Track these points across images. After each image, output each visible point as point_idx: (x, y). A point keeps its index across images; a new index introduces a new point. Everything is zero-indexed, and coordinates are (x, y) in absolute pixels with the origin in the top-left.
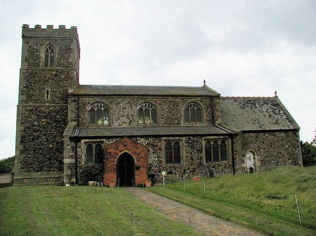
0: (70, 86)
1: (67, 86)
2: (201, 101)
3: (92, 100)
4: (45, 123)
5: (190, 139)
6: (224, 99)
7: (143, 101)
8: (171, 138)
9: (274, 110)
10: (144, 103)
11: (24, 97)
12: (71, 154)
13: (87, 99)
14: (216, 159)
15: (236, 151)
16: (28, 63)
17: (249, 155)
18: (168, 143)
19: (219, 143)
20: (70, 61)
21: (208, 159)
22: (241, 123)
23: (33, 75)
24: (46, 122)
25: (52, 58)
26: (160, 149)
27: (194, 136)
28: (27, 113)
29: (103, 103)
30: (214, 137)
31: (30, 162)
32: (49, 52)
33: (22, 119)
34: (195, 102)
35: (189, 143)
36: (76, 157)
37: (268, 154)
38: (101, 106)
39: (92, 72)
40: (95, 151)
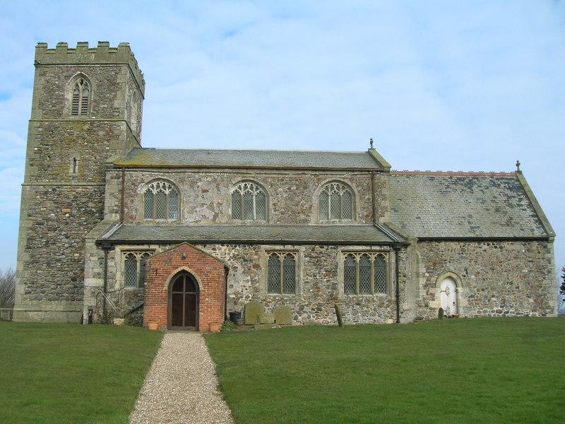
0: (115, 151)
1: (108, 151)
2: (351, 180)
3: (147, 175)
5: (313, 250)
6: (397, 174)
7: (240, 179)
8: (278, 247)
9: (509, 198)
10: (243, 181)
11: (35, 170)
13: (137, 175)
14: (366, 287)
15: (405, 276)
16: (43, 110)
17: (446, 284)
19: (373, 258)
20: (116, 104)
21: (350, 286)
22: (433, 219)
23: (51, 130)
24: (71, 215)
25: (85, 99)
26: (257, 266)
27: (322, 244)
28: (38, 197)
29: (169, 181)
31: (40, 282)
33: (29, 209)
34: (340, 181)
35: (311, 257)
36: (105, 275)
37: (485, 283)
38: (164, 187)
39: (166, 124)
40: (370, 275)
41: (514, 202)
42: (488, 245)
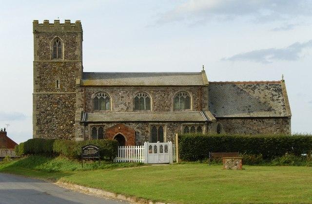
4: (56, 108)
5: (171, 125)
8: (156, 124)
12: (81, 134)
13: (92, 89)
18: (154, 128)
30: (191, 124)
32: (57, 45)
38: (103, 95)
39: (95, 58)
41: (275, 98)
42: (257, 120)
